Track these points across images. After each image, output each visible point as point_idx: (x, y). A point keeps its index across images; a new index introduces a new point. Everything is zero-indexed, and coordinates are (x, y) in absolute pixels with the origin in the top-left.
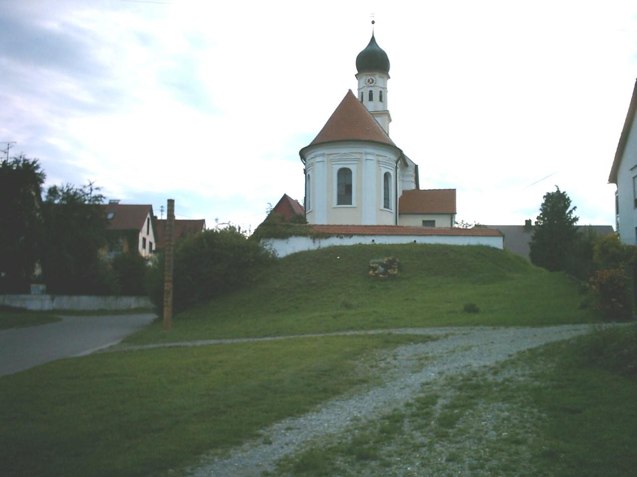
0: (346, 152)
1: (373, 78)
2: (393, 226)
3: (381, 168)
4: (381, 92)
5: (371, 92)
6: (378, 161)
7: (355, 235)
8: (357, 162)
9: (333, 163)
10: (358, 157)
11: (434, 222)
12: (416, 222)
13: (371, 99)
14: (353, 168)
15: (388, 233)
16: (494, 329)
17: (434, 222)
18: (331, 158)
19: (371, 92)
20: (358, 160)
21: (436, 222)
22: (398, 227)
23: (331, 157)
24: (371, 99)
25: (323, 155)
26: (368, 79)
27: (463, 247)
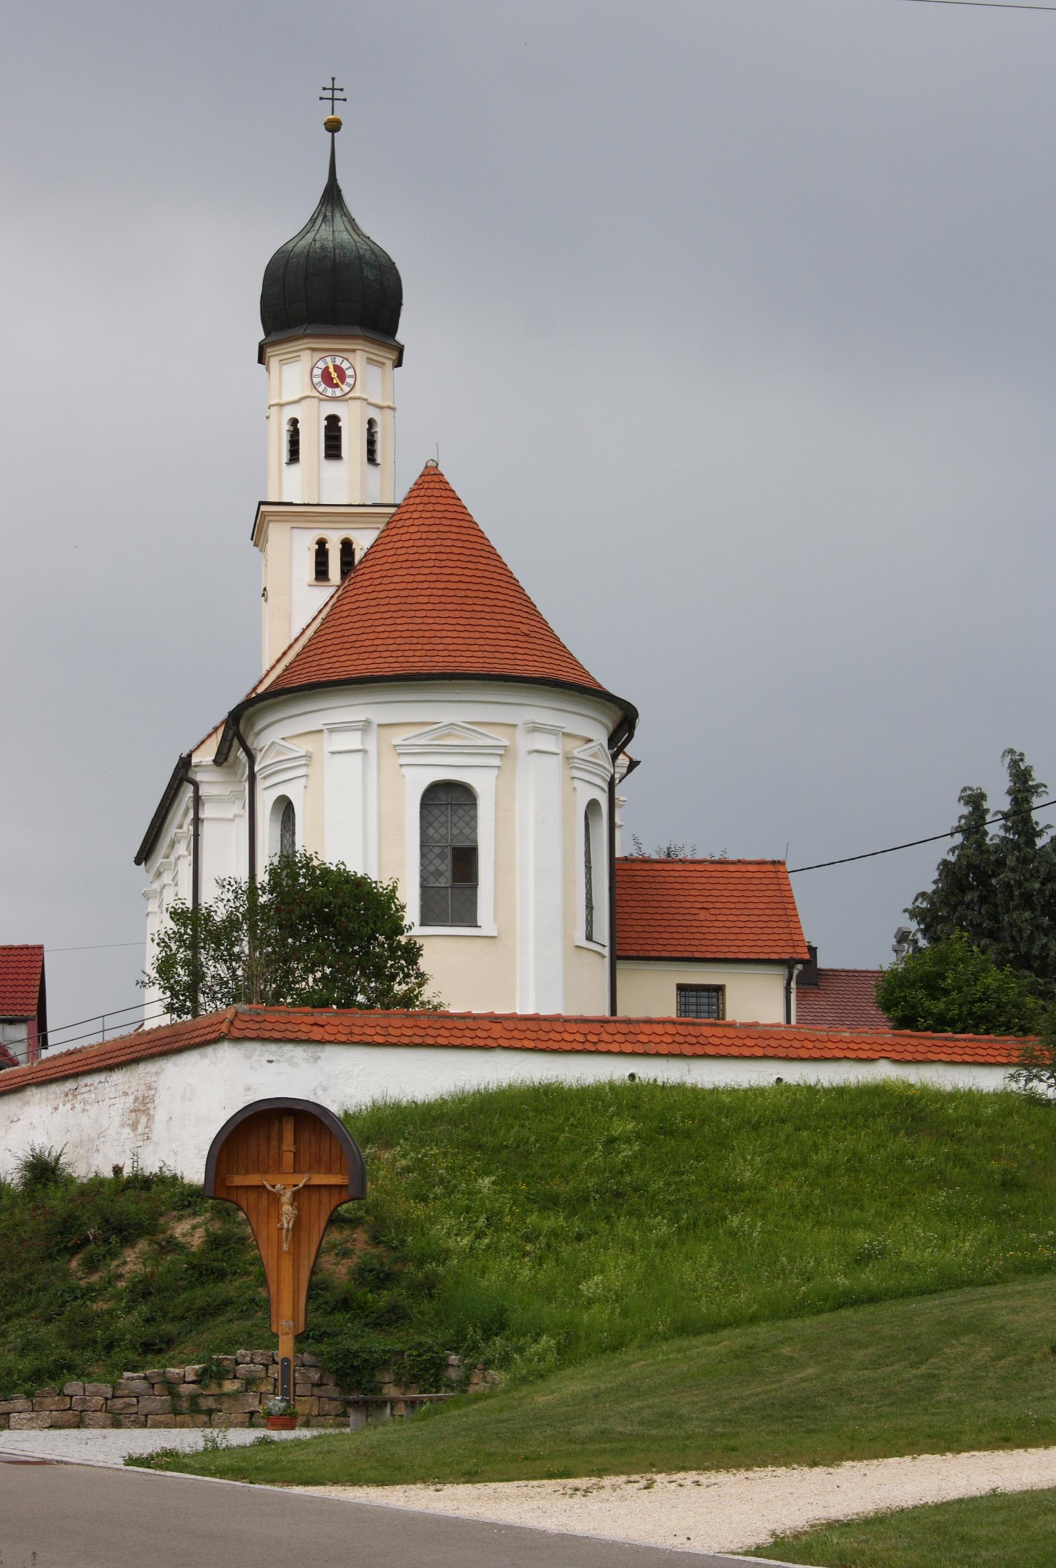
0: (457, 719)
1: (345, 365)
2: (602, 1021)
3: (577, 784)
4: (371, 423)
5: (333, 422)
6: (568, 758)
7: (28, 1085)
8: (496, 761)
9: (404, 760)
10: (505, 742)
11: (719, 989)
12: (653, 993)
13: (333, 449)
14: (482, 782)
15: (687, 1050)
16: (914, 1458)
17: (719, 989)
18: (397, 741)
19: (333, 422)
20: (505, 752)
21: (729, 994)
22: (628, 1022)
23: (398, 737)
24: (333, 449)
25: (365, 726)
26: (322, 365)
27: (758, 1092)
